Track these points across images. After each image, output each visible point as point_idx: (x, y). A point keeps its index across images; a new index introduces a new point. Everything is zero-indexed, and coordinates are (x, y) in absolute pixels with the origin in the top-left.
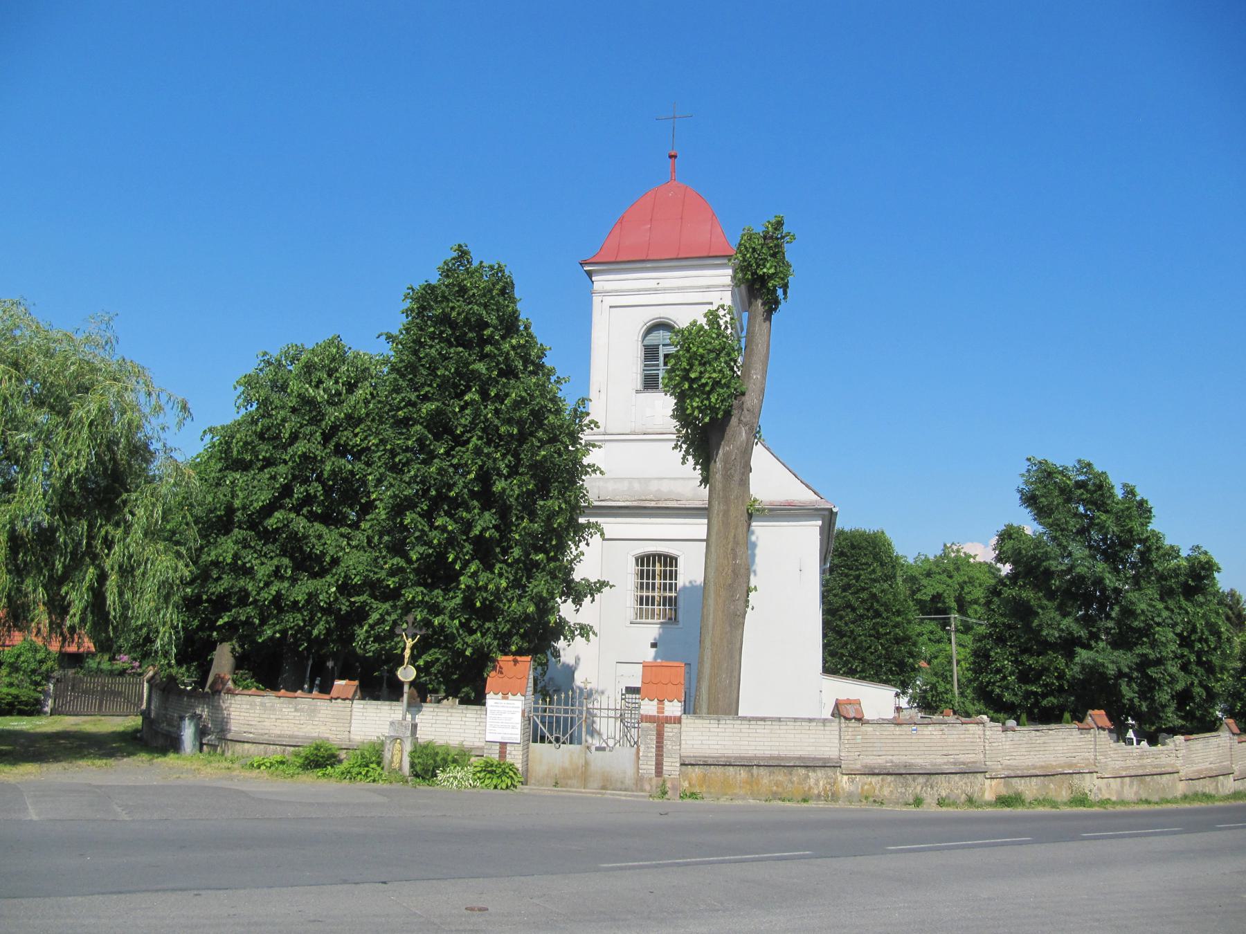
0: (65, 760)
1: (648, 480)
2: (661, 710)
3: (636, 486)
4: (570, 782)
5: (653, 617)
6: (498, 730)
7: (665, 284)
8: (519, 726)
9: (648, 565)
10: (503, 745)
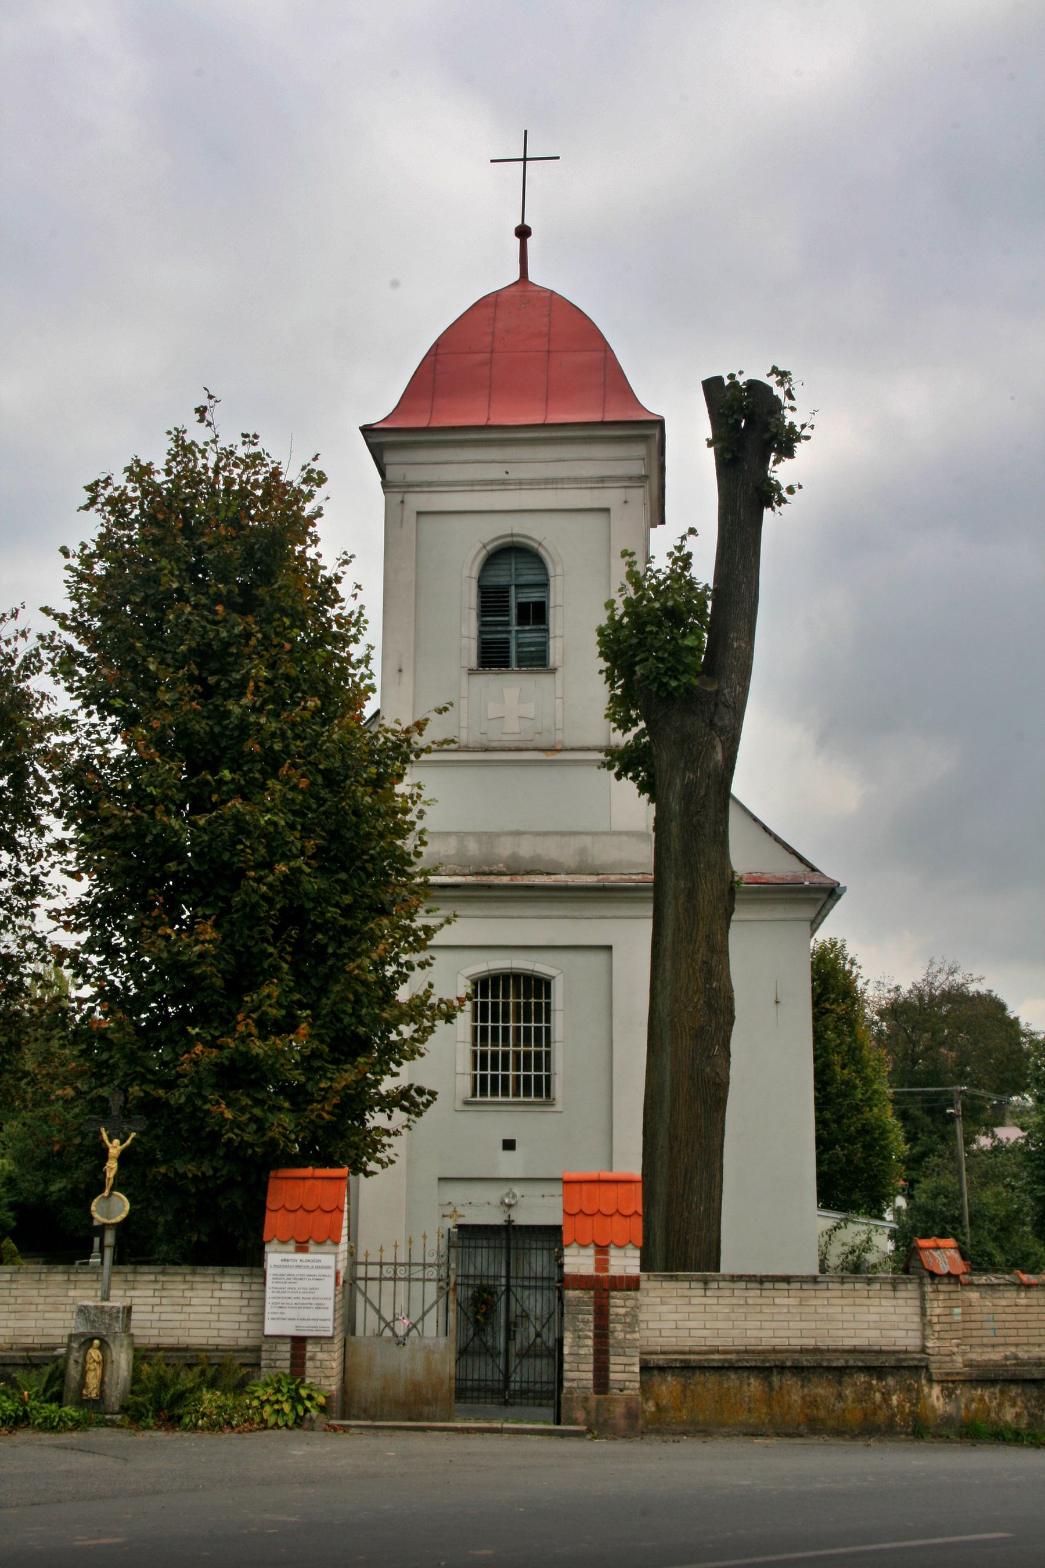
0: (211, 1270)
1: (491, 837)
2: (602, 1264)
3: (473, 847)
4: (426, 1410)
5: (527, 1094)
6: (290, 1313)
7: (518, 472)
8: (330, 1304)
9: (495, 996)
10: (299, 1343)
